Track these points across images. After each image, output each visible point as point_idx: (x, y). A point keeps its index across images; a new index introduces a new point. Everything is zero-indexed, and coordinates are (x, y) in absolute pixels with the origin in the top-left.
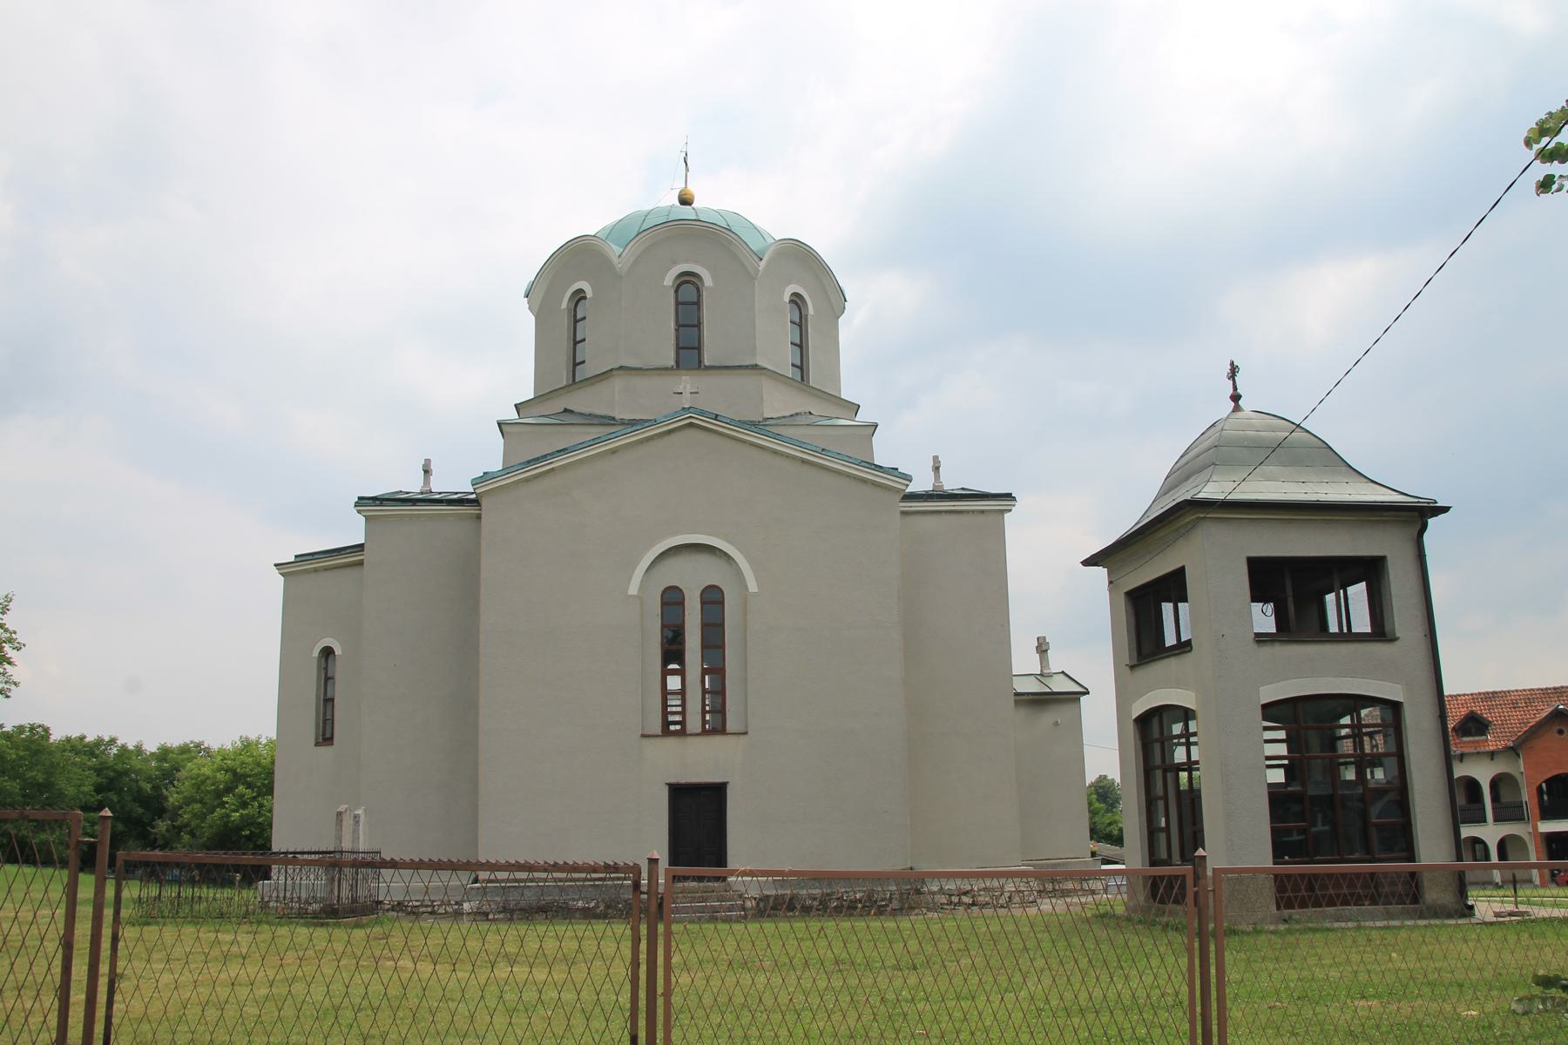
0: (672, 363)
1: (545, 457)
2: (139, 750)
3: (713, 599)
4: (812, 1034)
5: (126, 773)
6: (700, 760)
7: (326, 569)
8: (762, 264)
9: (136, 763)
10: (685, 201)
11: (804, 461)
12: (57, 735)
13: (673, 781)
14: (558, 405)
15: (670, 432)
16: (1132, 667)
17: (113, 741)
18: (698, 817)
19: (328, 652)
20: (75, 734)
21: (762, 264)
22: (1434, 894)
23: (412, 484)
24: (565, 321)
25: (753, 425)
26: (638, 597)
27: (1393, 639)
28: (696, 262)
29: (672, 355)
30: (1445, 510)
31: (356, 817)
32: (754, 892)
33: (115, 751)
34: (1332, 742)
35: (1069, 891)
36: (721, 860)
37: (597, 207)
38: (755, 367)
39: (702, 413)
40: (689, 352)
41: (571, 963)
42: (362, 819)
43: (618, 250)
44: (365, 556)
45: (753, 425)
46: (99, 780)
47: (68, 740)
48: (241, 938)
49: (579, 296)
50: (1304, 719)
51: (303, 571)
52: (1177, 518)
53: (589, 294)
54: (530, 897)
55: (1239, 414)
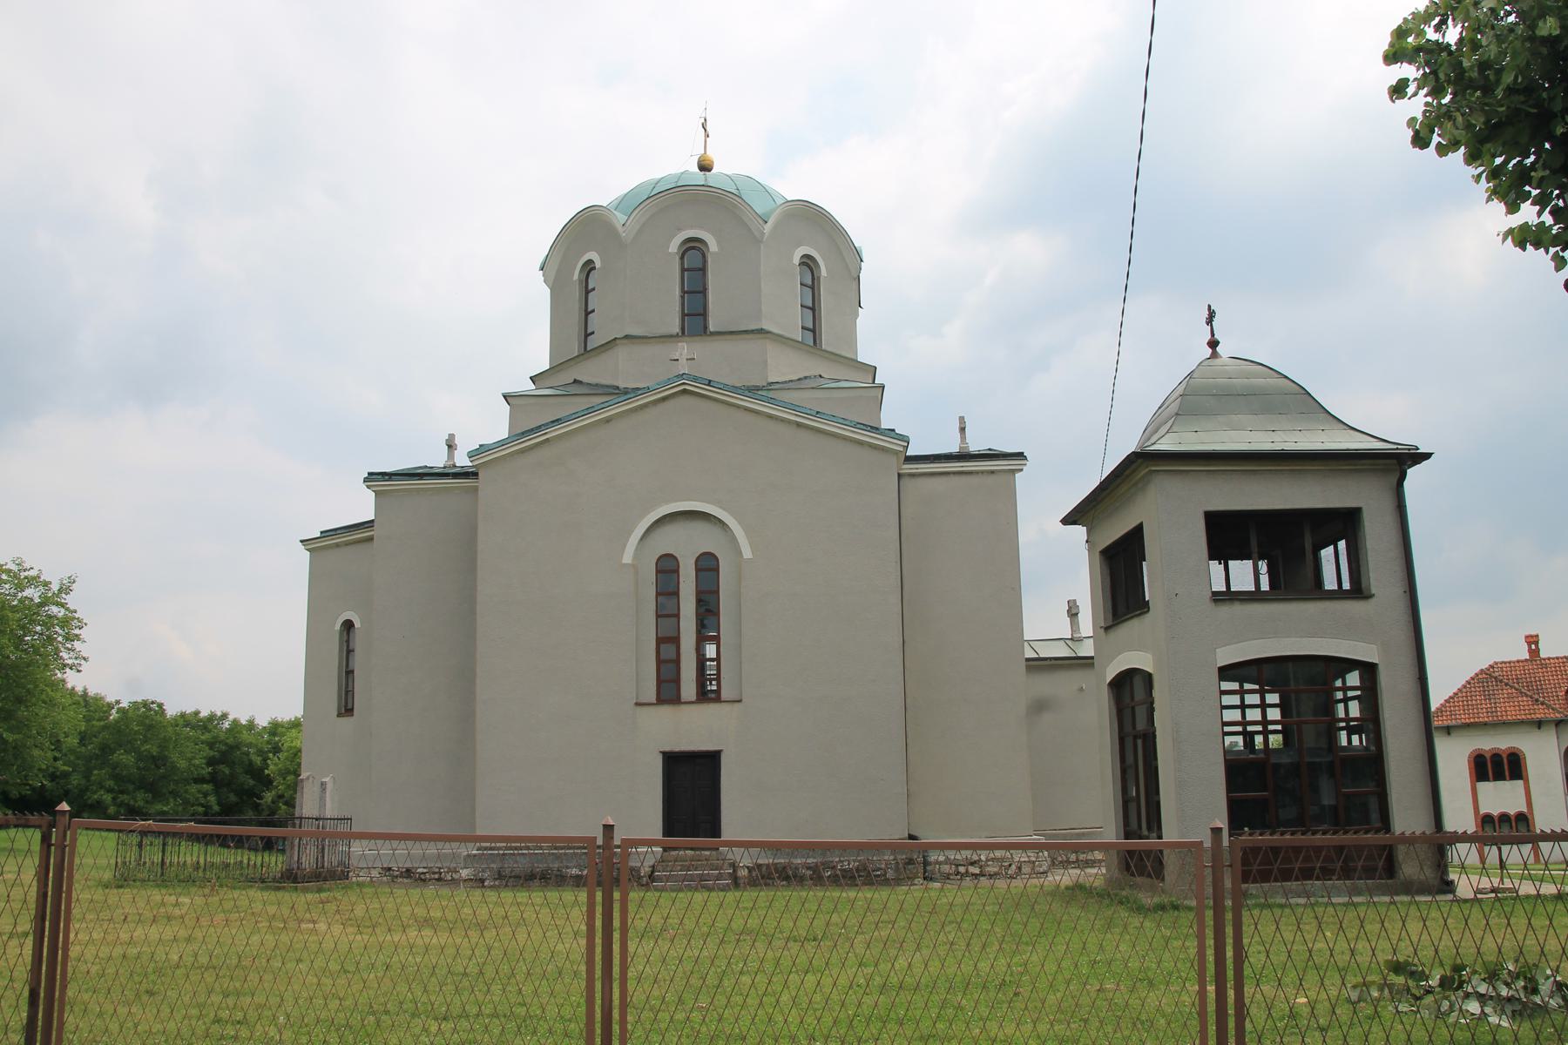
0: (676, 329)
1: (539, 428)
2: (251, 725)
3: (707, 566)
4: (430, 988)
5: (237, 747)
6: (692, 728)
7: (347, 544)
8: (768, 228)
9: (245, 737)
10: (705, 167)
11: (799, 425)
12: (171, 711)
13: (667, 749)
14: (567, 377)
15: (664, 399)
16: (1107, 629)
17: (224, 716)
18: (692, 786)
19: (348, 625)
20: (189, 710)
21: (768, 228)
22: (1409, 868)
23: (438, 460)
24: (576, 293)
25: (752, 391)
26: (633, 565)
27: (1370, 596)
28: (701, 228)
29: (677, 321)
30: (1427, 456)
31: (323, 784)
32: (747, 862)
33: (226, 725)
34: (1328, 707)
35: (1094, 862)
36: (716, 832)
37: (611, 182)
38: (761, 331)
39: (695, 379)
40: (695, 319)
41: (482, 929)
42: (329, 787)
43: (622, 218)
44: (375, 532)
45: (752, 391)
46: (212, 753)
47: (183, 715)
48: (257, 899)
49: (589, 267)
50: (1302, 682)
51: (331, 545)
52: (1139, 467)
53: (598, 264)
54: (522, 865)
55: (1217, 361)
